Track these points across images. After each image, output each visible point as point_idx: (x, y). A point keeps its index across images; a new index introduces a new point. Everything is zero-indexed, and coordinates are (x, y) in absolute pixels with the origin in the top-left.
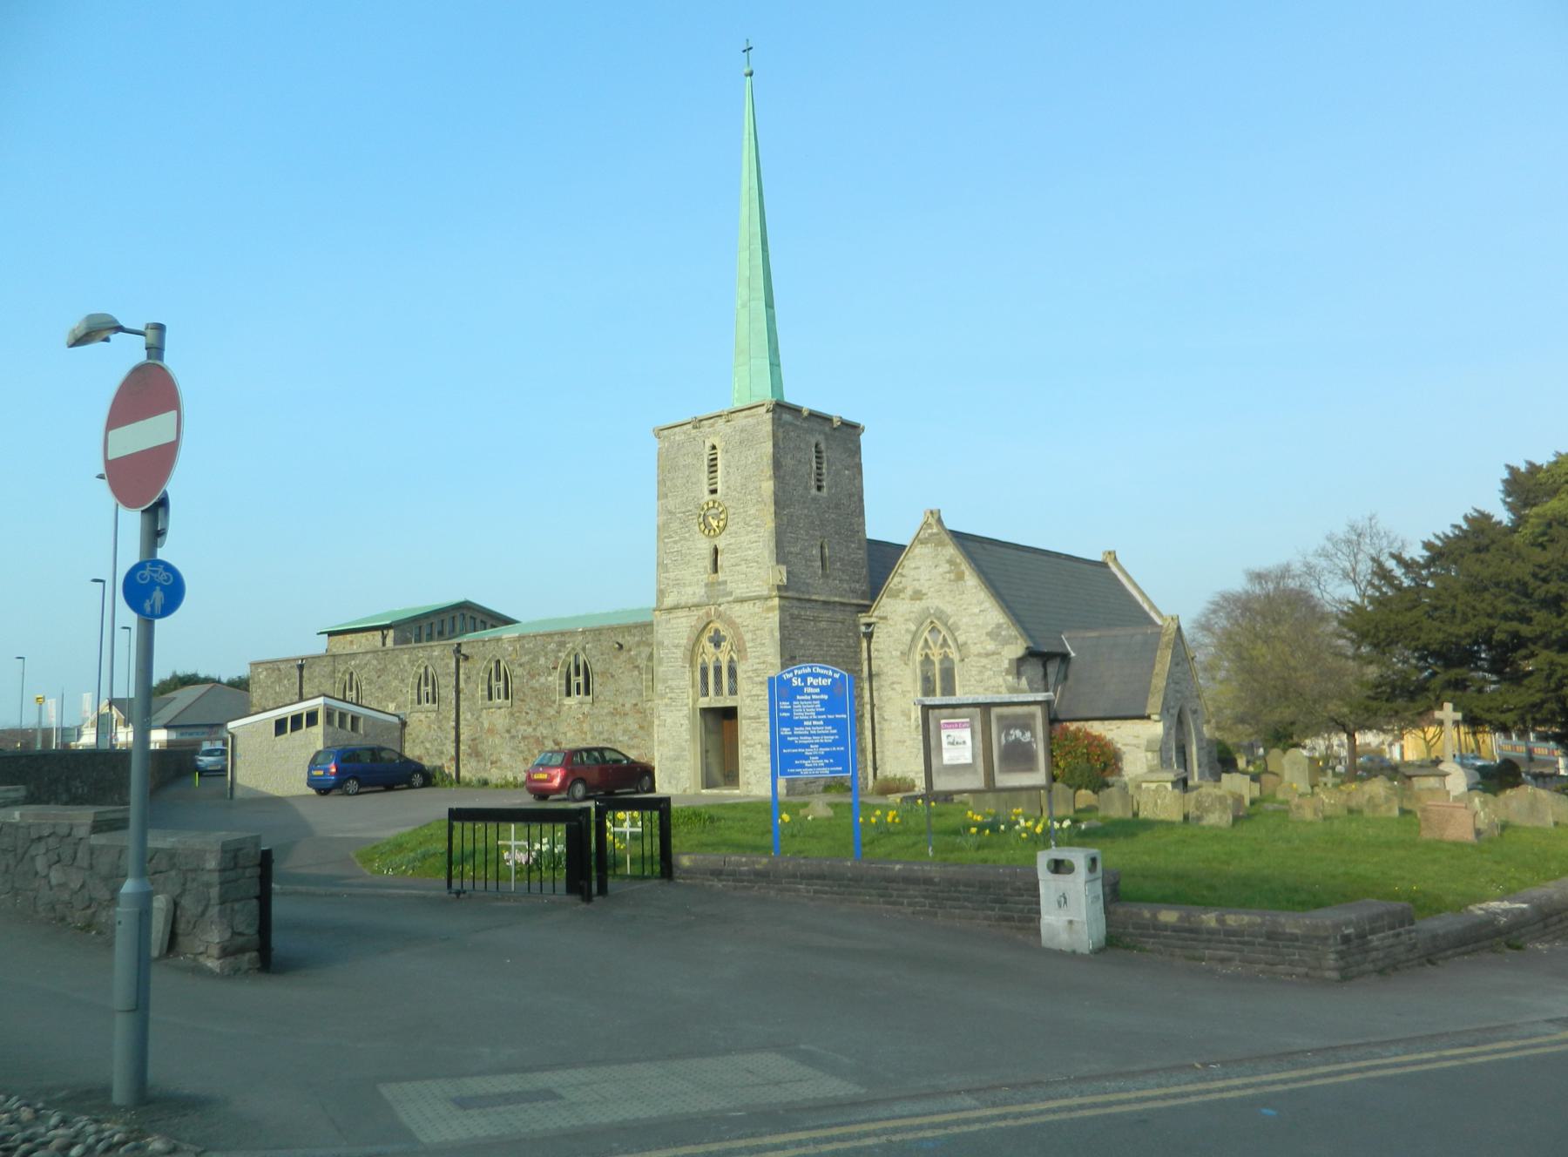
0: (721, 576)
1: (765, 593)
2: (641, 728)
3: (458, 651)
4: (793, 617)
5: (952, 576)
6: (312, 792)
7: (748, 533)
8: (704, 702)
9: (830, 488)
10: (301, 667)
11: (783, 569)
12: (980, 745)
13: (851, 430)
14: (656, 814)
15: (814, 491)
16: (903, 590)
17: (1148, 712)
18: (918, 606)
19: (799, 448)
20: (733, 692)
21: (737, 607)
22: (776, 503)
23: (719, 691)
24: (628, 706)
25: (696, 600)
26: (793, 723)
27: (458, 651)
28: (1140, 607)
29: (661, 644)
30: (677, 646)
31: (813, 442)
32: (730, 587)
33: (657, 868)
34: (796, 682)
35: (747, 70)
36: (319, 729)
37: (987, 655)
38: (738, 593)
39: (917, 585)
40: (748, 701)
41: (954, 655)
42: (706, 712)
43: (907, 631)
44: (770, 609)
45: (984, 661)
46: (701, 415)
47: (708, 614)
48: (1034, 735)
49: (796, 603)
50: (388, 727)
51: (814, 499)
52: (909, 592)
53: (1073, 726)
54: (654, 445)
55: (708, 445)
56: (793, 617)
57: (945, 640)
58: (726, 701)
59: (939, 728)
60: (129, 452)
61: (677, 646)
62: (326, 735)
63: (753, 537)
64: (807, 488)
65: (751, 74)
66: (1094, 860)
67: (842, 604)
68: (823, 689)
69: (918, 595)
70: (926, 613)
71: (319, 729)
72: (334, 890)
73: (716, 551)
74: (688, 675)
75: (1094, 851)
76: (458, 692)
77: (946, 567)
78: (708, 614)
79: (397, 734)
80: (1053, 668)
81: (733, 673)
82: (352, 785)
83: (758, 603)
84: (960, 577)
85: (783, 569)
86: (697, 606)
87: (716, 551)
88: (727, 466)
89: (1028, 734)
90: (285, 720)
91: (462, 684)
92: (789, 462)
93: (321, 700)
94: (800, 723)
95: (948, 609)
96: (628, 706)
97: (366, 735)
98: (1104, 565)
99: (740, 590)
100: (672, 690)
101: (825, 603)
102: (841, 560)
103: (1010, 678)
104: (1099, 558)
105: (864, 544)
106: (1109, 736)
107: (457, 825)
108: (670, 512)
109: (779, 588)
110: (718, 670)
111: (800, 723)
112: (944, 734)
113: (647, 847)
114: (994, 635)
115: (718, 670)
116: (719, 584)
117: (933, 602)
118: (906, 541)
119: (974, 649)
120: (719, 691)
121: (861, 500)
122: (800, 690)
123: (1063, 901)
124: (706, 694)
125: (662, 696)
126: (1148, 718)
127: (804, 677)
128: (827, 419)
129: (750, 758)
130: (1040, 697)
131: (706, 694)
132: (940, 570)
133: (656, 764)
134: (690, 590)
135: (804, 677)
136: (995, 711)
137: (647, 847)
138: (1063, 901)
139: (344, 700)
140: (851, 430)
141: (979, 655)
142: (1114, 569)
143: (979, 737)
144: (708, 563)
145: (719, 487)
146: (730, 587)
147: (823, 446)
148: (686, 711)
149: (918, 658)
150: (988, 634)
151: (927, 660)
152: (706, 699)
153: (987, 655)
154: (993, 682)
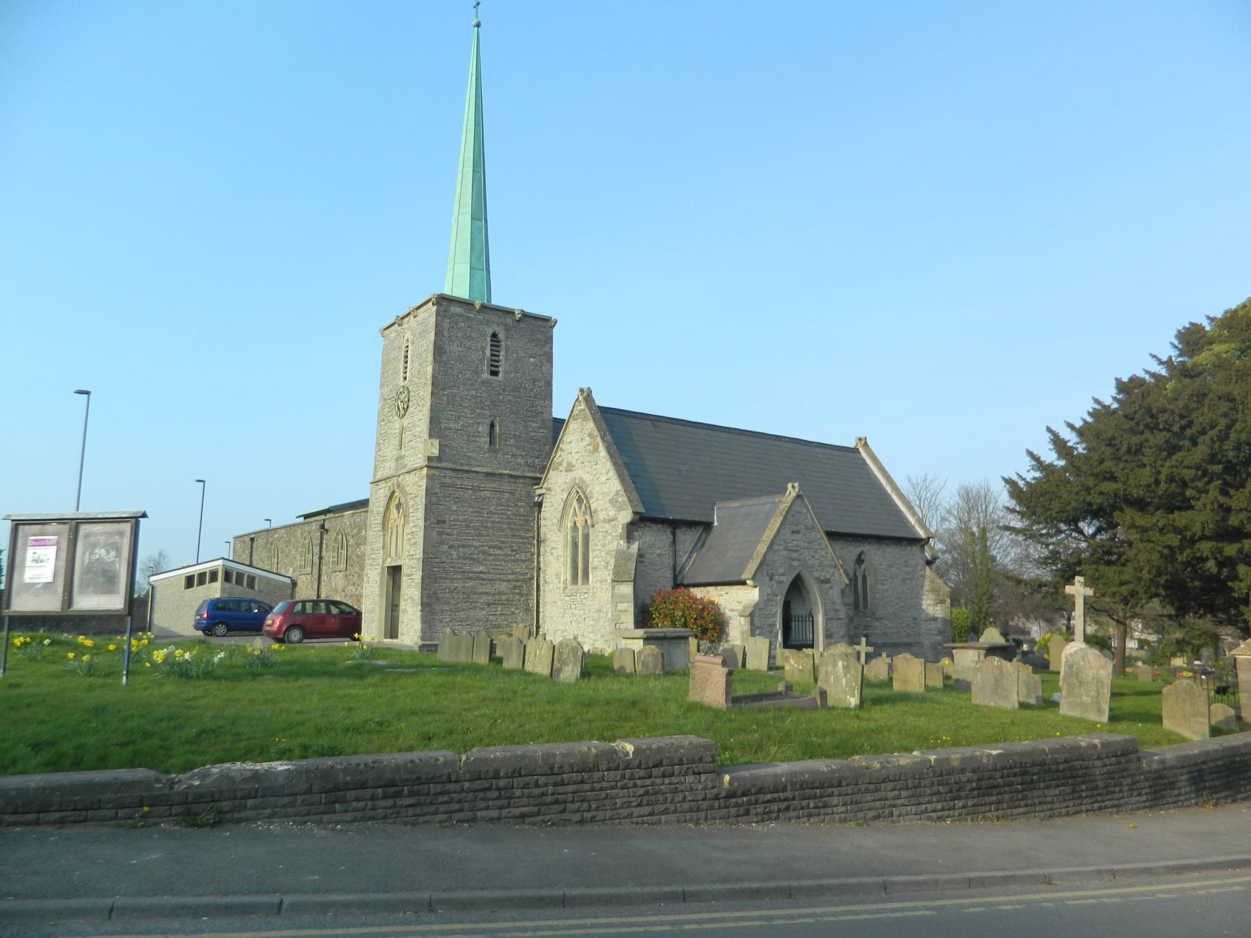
0: (403, 452)
3: (322, 527)
4: (443, 486)
5: (591, 448)
6: (200, 633)
9: (506, 373)
10: (252, 540)
11: (436, 442)
12: (63, 563)
13: (545, 324)
15: (486, 376)
17: (743, 577)
19: (470, 338)
22: (433, 384)
27: (322, 527)
28: (884, 489)
31: (489, 332)
35: (474, 22)
36: (217, 586)
46: (401, 314)
48: (118, 555)
49: (450, 473)
50: (281, 586)
51: (485, 383)
52: (565, 464)
53: (698, 593)
54: (380, 342)
56: (443, 486)
59: (25, 545)
62: (223, 590)
64: (477, 373)
65: (478, 25)
67: (511, 476)
71: (217, 586)
76: (321, 558)
79: (289, 592)
82: (221, 629)
84: (596, 449)
85: (436, 442)
89: (113, 553)
90: (204, 574)
91: (324, 553)
92: (454, 348)
93: (220, 562)
97: (260, 592)
98: (855, 450)
101: (488, 474)
102: (516, 437)
104: (851, 444)
105: (550, 424)
106: (717, 600)
109: (430, 459)
112: (30, 551)
114: (613, 502)
117: (579, 473)
118: (566, 418)
121: (549, 384)
126: (743, 583)
128: (510, 313)
136: (84, 529)
139: (251, 565)
140: (545, 324)
142: (864, 454)
143: (64, 555)
147: (501, 336)
149: (570, 524)
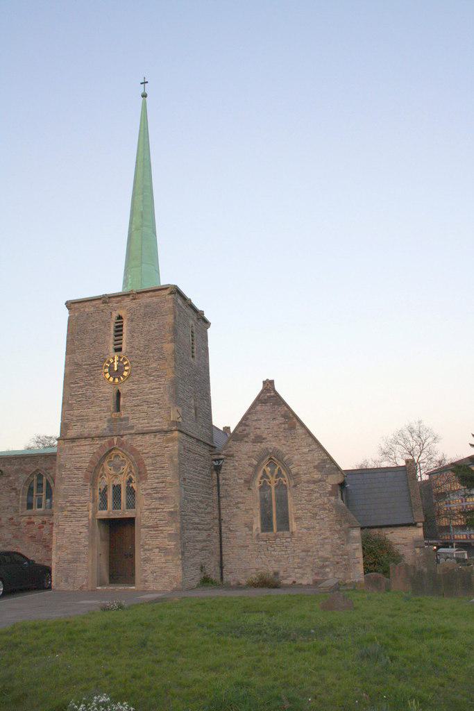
0: (123, 414)
1: (165, 427)
2: (15, 537)
7: (149, 382)
8: (103, 514)
16: (247, 435)
18: (259, 447)
20: (131, 505)
21: (139, 438)
23: (117, 505)
25: (99, 432)
29: (62, 466)
30: (78, 469)
32: (131, 422)
37: (314, 482)
38: (139, 427)
39: (258, 432)
40: (147, 513)
41: (285, 480)
42: (103, 521)
43: (250, 465)
44: (172, 440)
45: (312, 486)
47: (111, 443)
52: (252, 437)
54: (65, 314)
55: (115, 315)
57: (279, 470)
58: (128, 514)
61: (78, 469)
63: (154, 384)
69: (259, 439)
70: (266, 452)
73: (118, 394)
74: (88, 492)
77: (281, 420)
78: (111, 443)
83: (159, 436)
86: (100, 437)
87: (118, 394)
88: (132, 331)
95: (284, 449)
99: (141, 424)
100: (72, 504)
103: (333, 498)
108: (77, 364)
115: (117, 489)
116: (122, 420)
117: (272, 444)
119: (304, 478)
120: (117, 505)
124: (104, 507)
125: (62, 509)
129: (147, 560)
131: (104, 507)
132: (277, 422)
133: (54, 566)
134: (93, 424)
141: (308, 482)
144: (111, 403)
145: (124, 346)
146: (131, 422)
148: (85, 521)
149: (258, 485)
150: (315, 467)
151: (264, 487)
152: (104, 512)
153: (314, 482)
154: (320, 501)
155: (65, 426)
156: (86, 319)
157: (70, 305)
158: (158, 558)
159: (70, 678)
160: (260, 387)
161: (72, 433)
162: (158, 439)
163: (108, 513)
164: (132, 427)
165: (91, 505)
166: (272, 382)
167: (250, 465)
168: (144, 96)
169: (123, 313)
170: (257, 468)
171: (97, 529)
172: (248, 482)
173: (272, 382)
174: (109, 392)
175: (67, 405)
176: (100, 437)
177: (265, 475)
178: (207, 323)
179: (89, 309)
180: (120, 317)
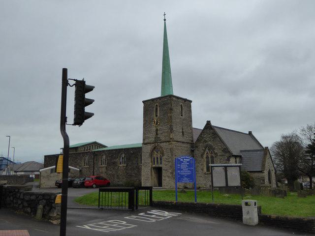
14: (149, 190)
20: (161, 163)
24: (135, 167)
26: (181, 170)
33: (149, 204)
34: (182, 160)
43: (203, 150)
58: (160, 166)
60: (60, 120)
66: (255, 203)
68: (188, 162)
69: (205, 141)
72: (156, 163)
75: (256, 201)
80: (238, 159)
81: (161, 159)
87: (157, 130)
94: (182, 170)
96: (135, 167)
107: (101, 193)
110: (157, 158)
111: (182, 170)
113: (146, 198)
115: (157, 158)
122: (182, 162)
123: (248, 213)
127: (183, 159)
130: (239, 165)
134: (151, 139)
135: (183, 159)
137: (146, 198)
138: (248, 213)
145: (158, 115)
149: (205, 156)
151: (207, 157)
155: (144, 140)
156: (149, 105)
157: (143, 102)
158: (167, 179)
159: (250, 218)
160: (205, 123)
161: (146, 142)
162: (168, 143)
163: (156, 165)
164: (160, 140)
165: (151, 163)
166: (210, 121)
167: (203, 150)
168: (165, 20)
169: (157, 104)
170: (204, 151)
171: (153, 170)
172: (202, 156)
173: (210, 121)
174: (155, 129)
175: (144, 134)
176: (153, 143)
177: (207, 153)
178: (95, 144)
179: (149, 103)
180: (157, 106)
